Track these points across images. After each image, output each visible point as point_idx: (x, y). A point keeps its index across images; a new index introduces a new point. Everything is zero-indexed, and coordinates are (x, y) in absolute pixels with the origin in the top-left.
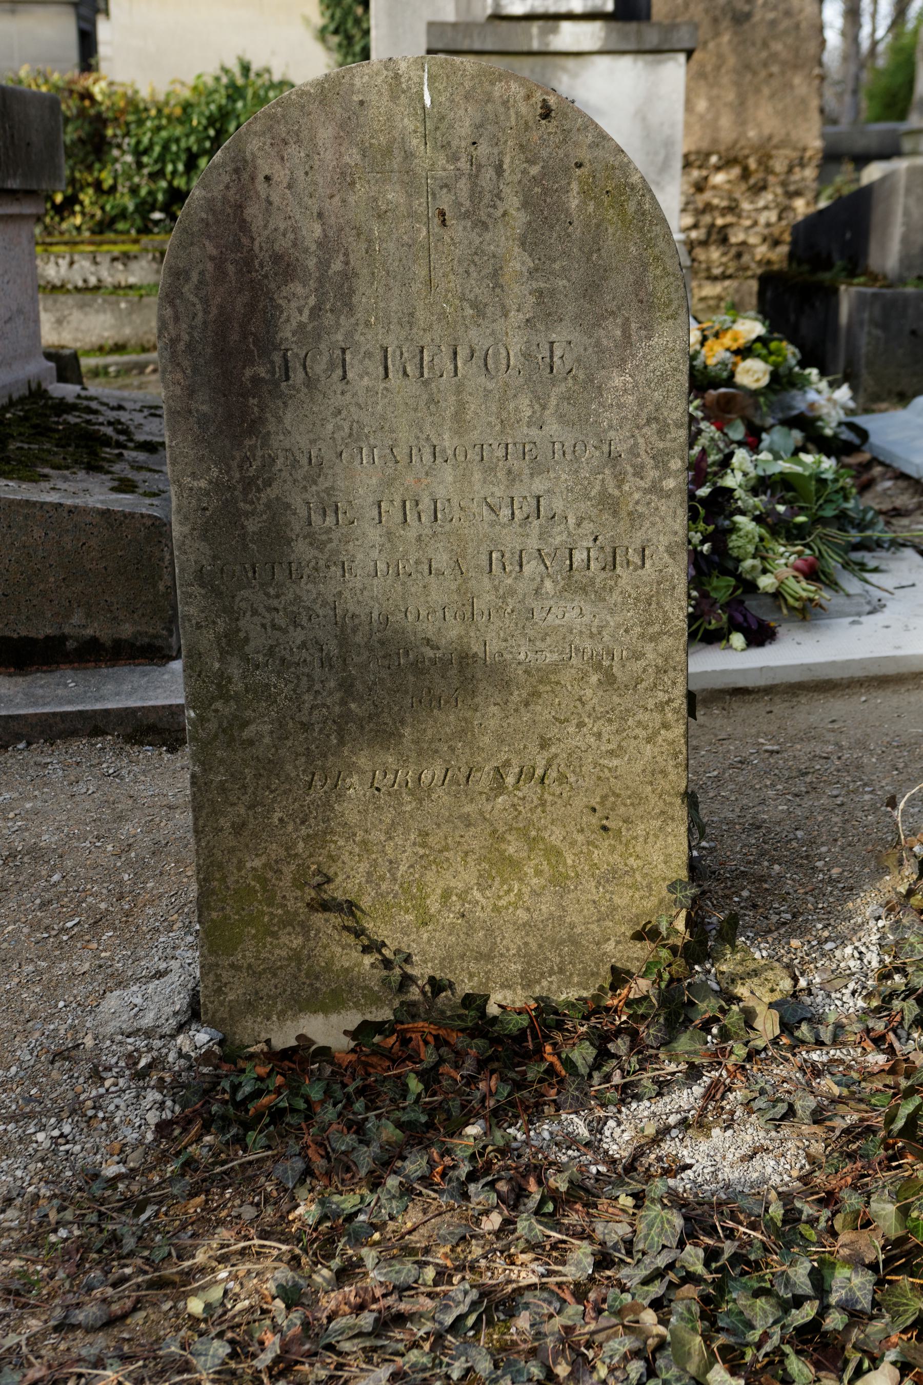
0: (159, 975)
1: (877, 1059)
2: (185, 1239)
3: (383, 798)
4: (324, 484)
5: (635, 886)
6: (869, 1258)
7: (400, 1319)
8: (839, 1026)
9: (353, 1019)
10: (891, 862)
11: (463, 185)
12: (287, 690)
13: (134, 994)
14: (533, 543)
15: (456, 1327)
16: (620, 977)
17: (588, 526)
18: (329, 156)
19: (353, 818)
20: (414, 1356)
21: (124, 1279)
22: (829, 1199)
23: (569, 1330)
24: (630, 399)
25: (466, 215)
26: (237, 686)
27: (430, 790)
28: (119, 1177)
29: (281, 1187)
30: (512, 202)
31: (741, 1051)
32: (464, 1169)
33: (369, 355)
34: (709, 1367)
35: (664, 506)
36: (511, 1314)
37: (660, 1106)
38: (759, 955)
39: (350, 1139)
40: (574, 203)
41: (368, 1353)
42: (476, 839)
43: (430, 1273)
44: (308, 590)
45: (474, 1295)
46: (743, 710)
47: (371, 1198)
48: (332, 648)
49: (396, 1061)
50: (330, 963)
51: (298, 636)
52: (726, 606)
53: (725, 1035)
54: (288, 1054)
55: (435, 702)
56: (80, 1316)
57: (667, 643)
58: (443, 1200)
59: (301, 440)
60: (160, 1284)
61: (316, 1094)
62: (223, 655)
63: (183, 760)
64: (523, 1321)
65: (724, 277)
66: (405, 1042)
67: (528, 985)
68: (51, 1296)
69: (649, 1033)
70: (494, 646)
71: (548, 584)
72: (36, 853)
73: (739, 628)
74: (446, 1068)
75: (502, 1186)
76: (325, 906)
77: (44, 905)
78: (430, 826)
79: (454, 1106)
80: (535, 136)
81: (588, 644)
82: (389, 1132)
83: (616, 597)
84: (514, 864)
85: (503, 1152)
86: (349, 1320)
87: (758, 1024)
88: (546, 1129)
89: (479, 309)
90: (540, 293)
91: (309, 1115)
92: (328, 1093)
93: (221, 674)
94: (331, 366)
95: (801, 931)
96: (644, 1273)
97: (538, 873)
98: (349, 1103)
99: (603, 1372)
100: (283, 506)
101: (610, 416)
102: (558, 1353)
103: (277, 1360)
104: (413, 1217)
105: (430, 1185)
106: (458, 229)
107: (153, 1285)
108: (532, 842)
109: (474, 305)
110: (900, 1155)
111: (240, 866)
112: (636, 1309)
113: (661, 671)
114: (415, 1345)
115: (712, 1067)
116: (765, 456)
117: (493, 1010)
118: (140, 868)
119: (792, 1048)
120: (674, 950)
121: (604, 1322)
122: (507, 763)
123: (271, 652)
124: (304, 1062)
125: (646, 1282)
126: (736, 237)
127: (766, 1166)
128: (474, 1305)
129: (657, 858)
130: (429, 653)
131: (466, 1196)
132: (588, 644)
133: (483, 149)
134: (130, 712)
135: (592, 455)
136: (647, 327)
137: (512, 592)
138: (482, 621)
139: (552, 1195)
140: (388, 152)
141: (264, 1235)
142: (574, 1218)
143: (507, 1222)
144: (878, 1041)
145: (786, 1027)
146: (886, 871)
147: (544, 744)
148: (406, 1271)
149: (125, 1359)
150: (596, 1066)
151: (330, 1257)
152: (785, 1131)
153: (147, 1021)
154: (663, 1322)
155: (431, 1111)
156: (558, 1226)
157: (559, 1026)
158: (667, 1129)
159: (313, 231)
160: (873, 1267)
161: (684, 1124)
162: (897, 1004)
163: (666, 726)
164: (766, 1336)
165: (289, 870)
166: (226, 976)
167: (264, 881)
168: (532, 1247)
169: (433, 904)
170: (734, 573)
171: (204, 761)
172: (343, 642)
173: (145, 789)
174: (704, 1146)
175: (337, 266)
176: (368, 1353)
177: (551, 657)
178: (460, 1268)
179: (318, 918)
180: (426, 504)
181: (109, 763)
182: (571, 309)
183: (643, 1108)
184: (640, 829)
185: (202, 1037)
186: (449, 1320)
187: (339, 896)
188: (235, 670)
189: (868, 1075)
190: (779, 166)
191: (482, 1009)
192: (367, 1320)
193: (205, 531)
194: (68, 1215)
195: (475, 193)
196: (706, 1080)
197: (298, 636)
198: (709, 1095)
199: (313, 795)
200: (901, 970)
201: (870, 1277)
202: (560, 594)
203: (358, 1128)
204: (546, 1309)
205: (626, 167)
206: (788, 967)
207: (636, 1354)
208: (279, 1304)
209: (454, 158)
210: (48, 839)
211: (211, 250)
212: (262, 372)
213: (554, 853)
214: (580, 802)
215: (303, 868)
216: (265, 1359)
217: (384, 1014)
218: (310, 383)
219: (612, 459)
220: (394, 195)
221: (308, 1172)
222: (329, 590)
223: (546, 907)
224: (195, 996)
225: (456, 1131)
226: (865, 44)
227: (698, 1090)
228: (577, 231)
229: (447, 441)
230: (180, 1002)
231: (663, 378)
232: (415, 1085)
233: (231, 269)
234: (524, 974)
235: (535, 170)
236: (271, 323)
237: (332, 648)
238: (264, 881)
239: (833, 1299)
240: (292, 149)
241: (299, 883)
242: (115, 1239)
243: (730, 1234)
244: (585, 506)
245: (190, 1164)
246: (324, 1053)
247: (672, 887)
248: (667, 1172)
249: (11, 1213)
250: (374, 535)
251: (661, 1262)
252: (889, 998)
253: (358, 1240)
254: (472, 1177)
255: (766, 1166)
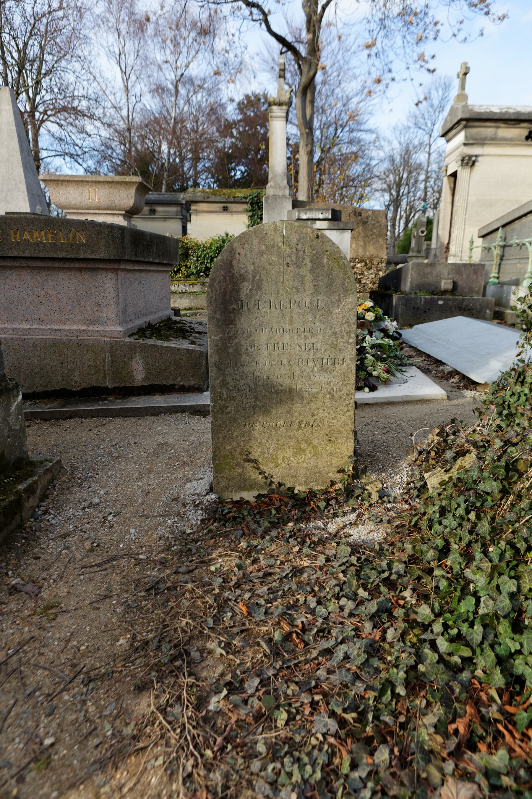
0: (201, 479)
1: (406, 507)
2: (209, 550)
3: (266, 430)
4: (251, 338)
5: (338, 457)
6: (404, 560)
7: (270, 574)
8: (395, 498)
9: (256, 493)
10: (410, 452)
11: (294, 256)
12: (239, 398)
13: (194, 484)
14: (311, 357)
15: (286, 576)
16: (333, 483)
17: (327, 352)
18: (256, 248)
19: (257, 435)
20: (274, 584)
21: (193, 561)
22: (392, 544)
23: (318, 578)
24: (340, 316)
25: (294, 264)
26: (225, 396)
27: (280, 428)
28: (191, 533)
29: (236, 538)
30: (308, 261)
31: (367, 504)
32: (288, 535)
33: (266, 302)
34: (358, 589)
35: (349, 347)
36: (301, 574)
37: (344, 519)
38: (373, 477)
39: (256, 526)
40: (325, 261)
41: (261, 583)
42: (292, 442)
43: (278, 562)
44: (246, 369)
45: (291, 568)
46: (368, 410)
47: (262, 542)
48: (252, 386)
49: (268, 505)
50: (250, 477)
51: (243, 382)
52: (364, 380)
53: (363, 500)
54: (237, 502)
55: (281, 402)
56: (181, 570)
57: (349, 387)
58: (282, 543)
59: (246, 326)
60: (203, 562)
61: (246, 513)
62: (221, 387)
63: (209, 419)
64: (305, 575)
65: (360, 292)
66: (271, 500)
67: (306, 485)
68: (173, 564)
69: (341, 499)
70: (299, 386)
71: (315, 369)
72: (167, 444)
73: (367, 386)
74: (283, 507)
75: (299, 540)
76: (249, 461)
77: (169, 458)
78: (279, 439)
79: (285, 518)
80: (314, 243)
81: (326, 387)
82: (267, 524)
83: (335, 373)
84: (303, 450)
85: (299, 530)
86: (256, 574)
87: (372, 497)
88: (311, 525)
89: (297, 290)
90: (315, 286)
91: (244, 519)
92: (249, 513)
93: (221, 393)
94: (255, 305)
95: (385, 471)
96: (339, 563)
97: (310, 453)
98: (255, 516)
99: (328, 590)
100: (239, 345)
101: (334, 321)
102: (315, 584)
103: (236, 584)
104: (273, 547)
105: (278, 539)
106: (292, 268)
107: (200, 562)
108: (309, 444)
109: (296, 289)
110: (412, 532)
111: (225, 448)
112: (337, 573)
113: (347, 395)
114: (274, 581)
115: (359, 508)
116: (374, 338)
117: (296, 492)
118: (195, 449)
119: (382, 503)
120: (349, 476)
121: (328, 576)
122: (302, 421)
123: (235, 387)
124: (242, 505)
125: (340, 566)
126: (363, 281)
127: (374, 535)
128: (291, 571)
129: (345, 449)
130: (280, 388)
131: (289, 542)
132: (326, 387)
133: (300, 246)
134: (193, 406)
135: (329, 332)
136: (346, 296)
137: (305, 371)
138: (296, 379)
139: (313, 542)
140: (273, 247)
141: (231, 550)
142: (319, 548)
143: (300, 549)
144: (406, 502)
145: (380, 498)
146: (409, 454)
147: (313, 415)
148: (272, 561)
149: (194, 582)
150: (326, 507)
151: (250, 557)
152: (380, 526)
153: (198, 491)
154: (345, 576)
155: (279, 519)
156: (315, 551)
157: (315, 496)
158: (346, 525)
159: (251, 268)
160: (405, 562)
161: (351, 524)
162: (412, 491)
163: (348, 411)
164: (374, 581)
165: (238, 450)
166: (220, 479)
167: (231, 453)
168: (307, 556)
169: (280, 461)
170: (366, 371)
171: (215, 418)
172: (256, 384)
173: (197, 428)
174: (356, 530)
175: (257, 277)
176: (261, 583)
177: (316, 390)
178: (287, 561)
179: (247, 464)
180: (281, 345)
181: (187, 420)
182: (324, 290)
183: (339, 519)
184: (340, 441)
185: (213, 496)
186: (284, 575)
187: (253, 458)
188: (224, 392)
189: (403, 511)
190: (375, 263)
191: (293, 492)
192: (261, 574)
193: (217, 352)
194: (177, 543)
195: (297, 258)
196: (357, 512)
197: (243, 382)
198: (358, 516)
199: (246, 429)
200: (413, 482)
201: (404, 565)
202: (319, 372)
203: (258, 523)
204: (311, 572)
205: (340, 252)
206: (381, 481)
207: (337, 585)
208: (236, 569)
209: (292, 249)
210: (170, 440)
211: (222, 273)
212: (235, 307)
213: (315, 447)
214: (323, 432)
215: (242, 450)
216: (232, 583)
217: (265, 492)
218: (249, 310)
219: (335, 333)
220: (274, 258)
221: (244, 534)
222: (252, 369)
223: (312, 463)
224: (211, 485)
225: (286, 524)
226: (397, 234)
227: (355, 515)
228: (326, 269)
229: (287, 327)
230: (207, 486)
231: (350, 310)
232: (274, 512)
233: (228, 278)
234: (305, 482)
235: (314, 252)
236: (238, 293)
237: (252, 386)
238: (231, 453)
239: (393, 571)
240: (246, 246)
241: (241, 454)
242: (190, 550)
243: (364, 553)
244: (327, 346)
245: (210, 531)
246: (248, 502)
247: (349, 458)
248: (346, 537)
249: (161, 542)
250: (265, 353)
251: (344, 560)
252: (409, 490)
253: (258, 552)
254: (290, 537)
255: (374, 535)
